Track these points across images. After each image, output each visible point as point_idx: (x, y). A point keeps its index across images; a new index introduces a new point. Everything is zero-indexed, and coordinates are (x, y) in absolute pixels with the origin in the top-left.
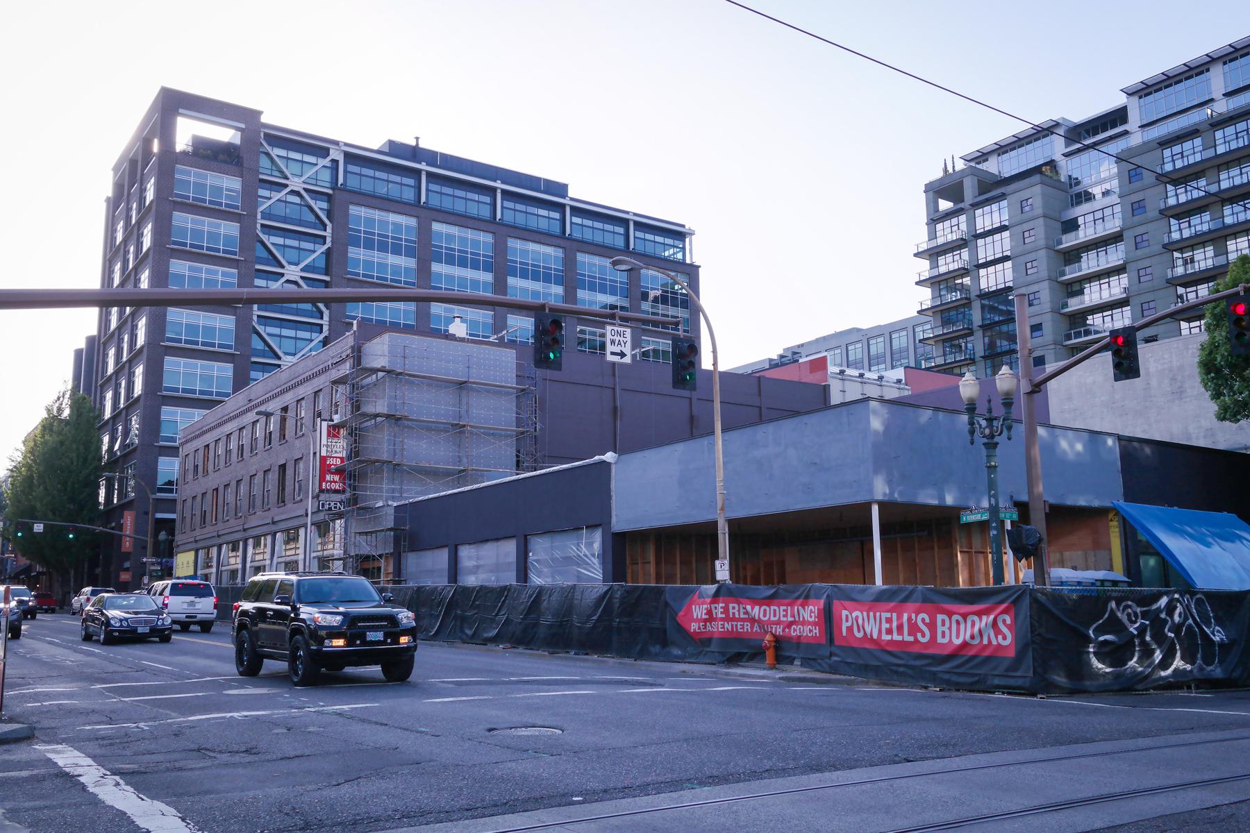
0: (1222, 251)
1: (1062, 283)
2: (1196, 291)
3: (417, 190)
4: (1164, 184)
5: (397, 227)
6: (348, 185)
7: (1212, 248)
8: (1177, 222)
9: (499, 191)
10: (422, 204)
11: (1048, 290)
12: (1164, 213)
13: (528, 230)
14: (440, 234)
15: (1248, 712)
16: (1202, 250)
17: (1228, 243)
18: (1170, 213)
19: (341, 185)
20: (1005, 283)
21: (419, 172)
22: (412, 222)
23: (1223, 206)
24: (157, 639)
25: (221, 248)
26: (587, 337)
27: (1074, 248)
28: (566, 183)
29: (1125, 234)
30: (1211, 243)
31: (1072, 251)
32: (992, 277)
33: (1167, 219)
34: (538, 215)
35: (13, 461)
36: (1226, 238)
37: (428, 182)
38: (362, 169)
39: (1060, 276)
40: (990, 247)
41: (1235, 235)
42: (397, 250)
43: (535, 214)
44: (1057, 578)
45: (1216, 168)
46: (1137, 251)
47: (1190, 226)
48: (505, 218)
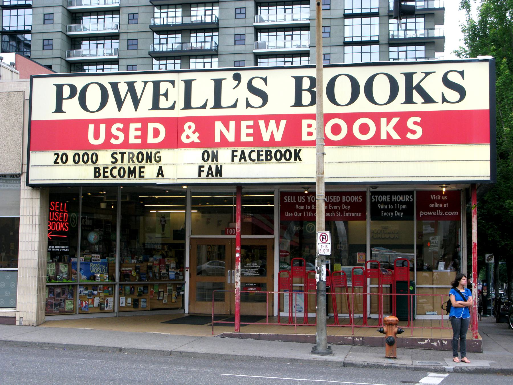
0: (186, 40)
1: (68, 36)
2: (167, 38)
4: (153, 6)
7: (181, 9)
8: (159, 11)
11: (61, 14)
12: (151, 55)
16: (174, 10)
17: (192, 9)
18: (154, 29)
20: (25, 26)
23: (190, 33)
27: (80, 62)
29: (122, 10)
30: (181, 6)
31: (69, 187)
32: (14, 19)
33: (151, 59)
36: (190, 57)
39: (68, 57)
40: (14, 19)
41: (196, 57)
44: (35, 192)
45: (189, 30)
46: (128, 51)
47: (167, 17)
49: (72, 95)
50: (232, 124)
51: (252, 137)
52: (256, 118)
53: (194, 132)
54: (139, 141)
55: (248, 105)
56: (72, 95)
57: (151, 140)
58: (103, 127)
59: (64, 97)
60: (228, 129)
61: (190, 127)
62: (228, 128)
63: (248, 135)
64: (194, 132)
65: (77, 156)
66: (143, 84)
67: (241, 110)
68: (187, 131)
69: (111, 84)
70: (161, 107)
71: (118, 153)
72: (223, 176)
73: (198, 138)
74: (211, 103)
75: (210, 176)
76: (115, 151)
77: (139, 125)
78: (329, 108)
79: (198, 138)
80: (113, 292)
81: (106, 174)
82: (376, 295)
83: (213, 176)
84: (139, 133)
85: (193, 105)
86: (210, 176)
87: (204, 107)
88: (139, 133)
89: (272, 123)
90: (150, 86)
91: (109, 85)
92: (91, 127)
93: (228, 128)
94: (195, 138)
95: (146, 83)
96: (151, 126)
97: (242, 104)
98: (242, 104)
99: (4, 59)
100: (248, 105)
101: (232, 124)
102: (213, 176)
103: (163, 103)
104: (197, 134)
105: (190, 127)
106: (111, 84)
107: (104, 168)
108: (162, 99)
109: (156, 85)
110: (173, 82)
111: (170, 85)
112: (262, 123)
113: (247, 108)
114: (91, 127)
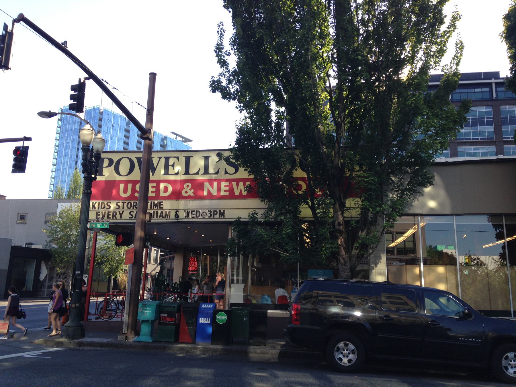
3: (491, 93)
5: (480, 113)
6: (498, 97)
9: (494, 85)
10: (494, 99)
13: (485, 101)
14: (505, 112)
15: (1, 311)
19: (495, 98)
21: (491, 84)
22: (490, 109)
24: (181, 281)
25: (510, 137)
26: (511, 150)
28: (12, 63)
34: (475, 92)
35: (381, 228)
37: (496, 87)
38: (483, 89)
42: (482, 124)
43: (473, 92)
48: (499, 96)
49: (110, 165)
50: (215, 184)
51: (155, 189)
52: (230, 181)
53: (190, 189)
54: (154, 195)
55: (226, 172)
56: (110, 165)
57: (162, 194)
58: (130, 186)
59: (104, 166)
60: (213, 188)
61: (188, 186)
62: (212, 186)
63: (225, 191)
64: (190, 189)
65: (129, 204)
66: (159, 158)
67: (222, 175)
68: (186, 189)
69: (137, 158)
70: (169, 173)
71: (121, 202)
72: (225, 217)
73: (193, 193)
74: (202, 171)
75: (161, 218)
76: (119, 201)
77: (155, 185)
78: (133, 157)
79: (193, 193)
80: (97, 307)
81: (110, 216)
82: (199, 345)
83: (163, 217)
84: (154, 190)
85: (190, 173)
86: (161, 218)
87: (197, 173)
88: (154, 190)
89: (241, 184)
90: (163, 160)
91: (136, 159)
92: (122, 186)
93: (212, 186)
94: (191, 193)
95: (160, 158)
96: (162, 186)
97: (222, 172)
98: (222, 172)
99: (32, 138)
100: (226, 172)
101: (215, 184)
102: (163, 217)
103: (171, 170)
104: (192, 191)
105: (188, 186)
106: (137, 158)
107: (192, 211)
108: (170, 168)
109: (167, 159)
110: (178, 158)
111: (176, 159)
112: (234, 184)
113: (225, 174)
114: (122, 186)
